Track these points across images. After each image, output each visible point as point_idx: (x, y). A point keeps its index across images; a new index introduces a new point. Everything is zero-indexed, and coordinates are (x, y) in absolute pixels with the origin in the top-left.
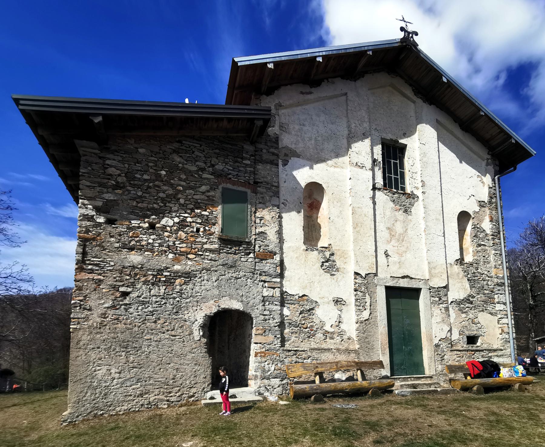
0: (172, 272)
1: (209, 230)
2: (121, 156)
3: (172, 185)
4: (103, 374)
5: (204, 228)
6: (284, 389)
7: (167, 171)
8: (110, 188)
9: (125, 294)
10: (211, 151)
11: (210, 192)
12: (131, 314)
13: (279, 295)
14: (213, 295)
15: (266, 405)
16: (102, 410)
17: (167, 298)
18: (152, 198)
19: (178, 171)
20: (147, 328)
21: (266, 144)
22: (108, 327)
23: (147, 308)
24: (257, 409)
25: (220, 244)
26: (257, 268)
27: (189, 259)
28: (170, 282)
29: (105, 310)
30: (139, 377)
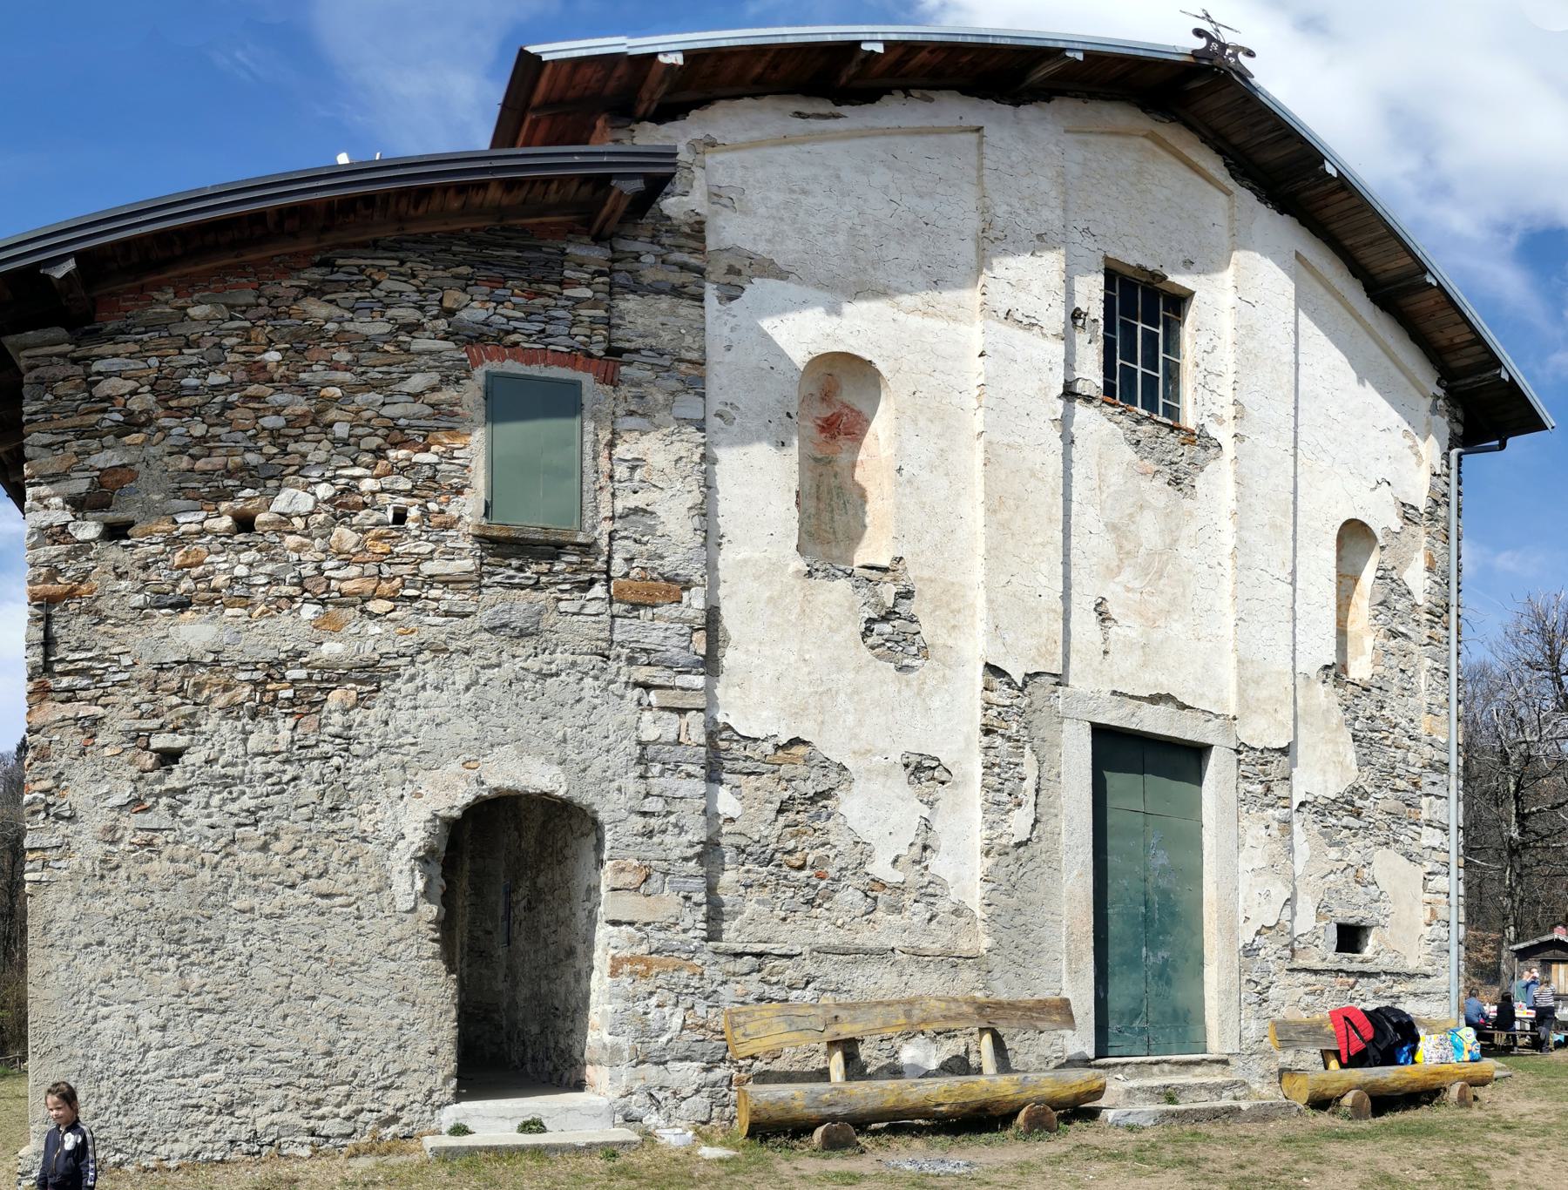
0: (314, 668)
1: (442, 512)
2: (136, 342)
3: (304, 388)
4: (118, 1033)
5: (424, 506)
6: (717, 1102)
7: (287, 350)
8: (108, 433)
9: (169, 758)
10: (440, 273)
11: (440, 390)
12: (188, 823)
13: (703, 740)
14: (457, 740)
15: (654, 1159)
16: (119, 1151)
17: (300, 760)
18: (239, 436)
19: (323, 345)
20: (239, 869)
21: (654, 239)
22: (122, 873)
23: (238, 798)
24: (620, 1173)
25: (481, 557)
26: (617, 637)
27: (373, 616)
28: (309, 703)
29: (114, 814)
30: (221, 1044)
